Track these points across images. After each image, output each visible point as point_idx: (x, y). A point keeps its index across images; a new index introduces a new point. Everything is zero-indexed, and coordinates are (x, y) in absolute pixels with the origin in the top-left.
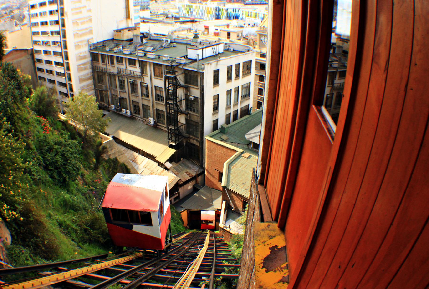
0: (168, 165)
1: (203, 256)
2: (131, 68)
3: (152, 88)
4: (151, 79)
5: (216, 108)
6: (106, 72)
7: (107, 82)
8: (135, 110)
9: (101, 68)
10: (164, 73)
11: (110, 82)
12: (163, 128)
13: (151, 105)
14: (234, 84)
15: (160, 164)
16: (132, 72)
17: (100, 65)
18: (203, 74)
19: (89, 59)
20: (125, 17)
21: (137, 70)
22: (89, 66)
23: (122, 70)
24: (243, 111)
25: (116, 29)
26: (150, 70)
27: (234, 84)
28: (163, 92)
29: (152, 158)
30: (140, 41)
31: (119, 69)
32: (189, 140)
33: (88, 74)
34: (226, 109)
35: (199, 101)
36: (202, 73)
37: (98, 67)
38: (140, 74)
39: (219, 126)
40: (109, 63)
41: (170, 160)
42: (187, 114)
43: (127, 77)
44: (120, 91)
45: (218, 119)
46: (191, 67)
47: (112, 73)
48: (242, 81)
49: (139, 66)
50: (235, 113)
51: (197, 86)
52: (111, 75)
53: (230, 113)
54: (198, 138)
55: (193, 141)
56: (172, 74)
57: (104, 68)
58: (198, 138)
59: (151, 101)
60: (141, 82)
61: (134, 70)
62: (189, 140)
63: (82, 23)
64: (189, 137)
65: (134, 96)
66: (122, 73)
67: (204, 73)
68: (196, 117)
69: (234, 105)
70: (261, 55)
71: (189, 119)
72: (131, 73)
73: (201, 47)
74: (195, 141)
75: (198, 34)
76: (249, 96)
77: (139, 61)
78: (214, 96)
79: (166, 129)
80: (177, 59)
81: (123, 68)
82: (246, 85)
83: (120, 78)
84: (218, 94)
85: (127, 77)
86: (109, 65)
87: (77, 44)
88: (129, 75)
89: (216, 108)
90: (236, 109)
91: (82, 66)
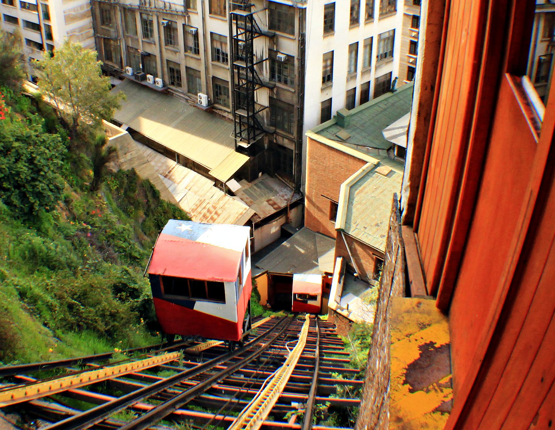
0: (234, 185)
3: (204, 35)
4: (204, 19)
5: (328, 78)
6: (116, 4)
10: (230, 7)
11: (124, 24)
12: (226, 114)
15: (218, 183)
16: (167, 5)
28: (226, 44)
32: (276, 139)
38: (182, 9)
39: (334, 113)
41: (238, 176)
43: (158, 14)
44: (142, 41)
45: (331, 100)
50: (365, 87)
51: (293, 33)
55: (283, 140)
60: (184, 25)
64: (275, 132)
66: (148, 5)
67: (306, 8)
69: (363, 73)
71: (275, 97)
74: (286, 141)
76: (393, 56)
79: (231, 117)
85: (158, 14)
88: (161, 11)
89: (328, 78)
90: (366, 80)
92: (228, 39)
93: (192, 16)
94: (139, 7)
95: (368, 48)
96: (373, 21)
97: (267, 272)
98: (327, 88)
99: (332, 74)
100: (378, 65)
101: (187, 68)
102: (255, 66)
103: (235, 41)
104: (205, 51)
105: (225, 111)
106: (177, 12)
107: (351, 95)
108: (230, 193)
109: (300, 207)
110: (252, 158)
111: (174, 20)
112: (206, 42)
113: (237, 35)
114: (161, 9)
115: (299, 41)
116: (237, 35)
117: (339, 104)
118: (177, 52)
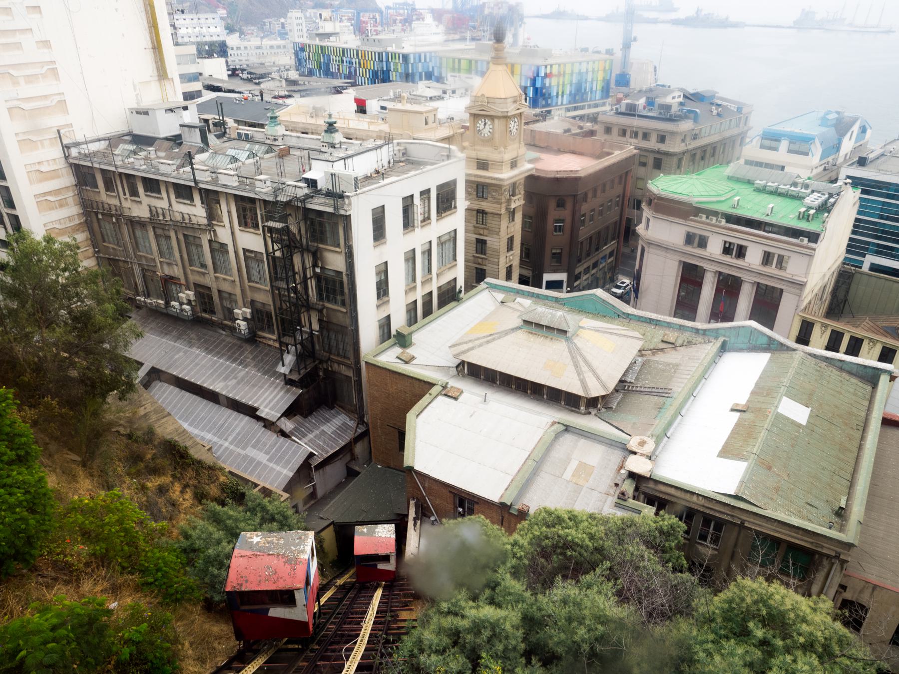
0: (288, 425)
1: (369, 631)
2: (181, 208)
3: (236, 253)
4: (233, 233)
5: (382, 289)
6: (120, 215)
7: (127, 238)
8: (203, 303)
9: (106, 206)
10: (262, 218)
11: (133, 241)
12: (271, 343)
13: (238, 291)
14: (420, 238)
15: (268, 424)
16: (186, 217)
17: (103, 196)
18: (347, 218)
19: (68, 180)
20: (156, 73)
21: (197, 211)
22: (70, 196)
23: (160, 211)
24: (444, 293)
25: (135, 106)
26: (229, 212)
27: (420, 238)
28: (263, 261)
29: (251, 412)
30: (199, 140)
31: (153, 209)
32: (331, 366)
33: (70, 218)
34: (406, 293)
35: (345, 279)
36: (346, 216)
37: (102, 203)
38: (205, 221)
39: (393, 332)
40: (125, 194)
41: (289, 413)
42: (320, 311)
43: (176, 228)
44: (161, 262)
45: (389, 317)
46: (319, 204)
47: (138, 219)
48: (439, 228)
49: (202, 203)
50: (428, 298)
51: (338, 246)
52: (135, 223)
53: (416, 301)
54: (349, 359)
55: (339, 366)
56: (280, 222)
57: (115, 206)
58: (349, 359)
59: (238, 283)
60: (210, 241)
61: (190, 213)
62: (331, 366)
63: (30, 79)
64: (329, 359)
65: (198, 272)
66: (161, 218)
67: (350, 215)
68: (341, 315)
69: (423, 283)
70: (478, 163)
71: (325, 319)
72: (183, 218)
73: (342, 155)
74: (342, 368)
75: (335, 123)
76: (456, 260)
77: (200, 190)
78: (373, 210)
79: (277, 345)
80: (288, 185)
81: (163, 207)
82: (447, 237)
83: (159, 232)
84: (383, 206)
85: (176, 228)
86: (126, 199)
87: (21, 137)
88: (179, 224)
89: (382, 289)
90: (427, 291)
91: (49, 198)
92: (265, 255)
93: (219, 230)
94: (151, 219)
95: (426, 256)
96: (430, 223)
97: (332, 523)
98: (383, 303)
99: (388, 288)
100: (439, 271)
101: (219, 291)
102: (299, 286)
103: (273, 260)
104: (238, 271)
105: (270, 339)
106: (199, 225)
107: (412, 308)
108: (283, 434)
109: (366, 440)
110: (305, 390)
111: (197, 235)
112: (240, 261)
113: (274, 251)
114: (178, 222)
115: (346, 253)
116: (274, 251)
117: (398, 323)
118: (206, 273)
